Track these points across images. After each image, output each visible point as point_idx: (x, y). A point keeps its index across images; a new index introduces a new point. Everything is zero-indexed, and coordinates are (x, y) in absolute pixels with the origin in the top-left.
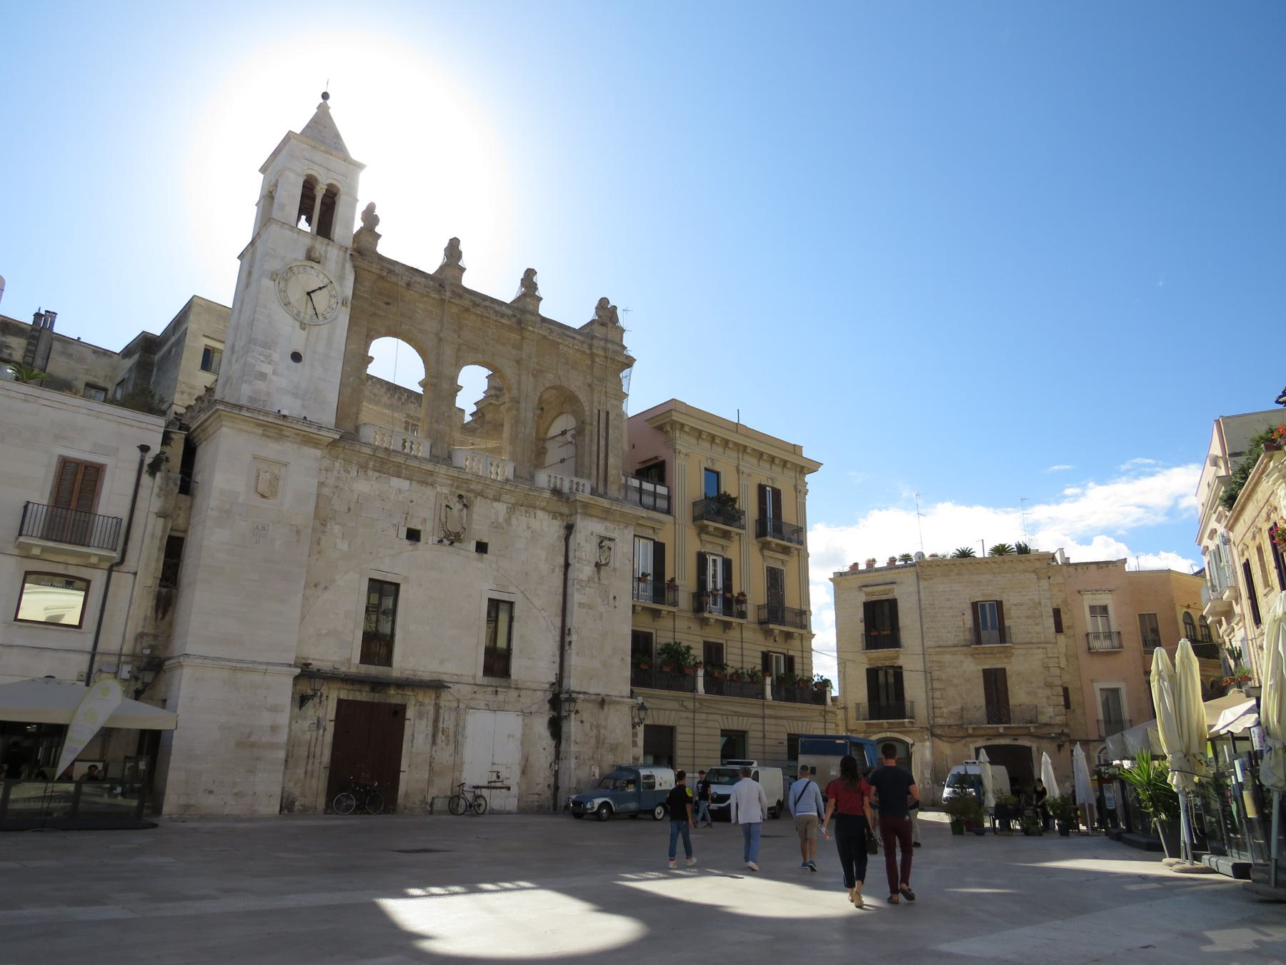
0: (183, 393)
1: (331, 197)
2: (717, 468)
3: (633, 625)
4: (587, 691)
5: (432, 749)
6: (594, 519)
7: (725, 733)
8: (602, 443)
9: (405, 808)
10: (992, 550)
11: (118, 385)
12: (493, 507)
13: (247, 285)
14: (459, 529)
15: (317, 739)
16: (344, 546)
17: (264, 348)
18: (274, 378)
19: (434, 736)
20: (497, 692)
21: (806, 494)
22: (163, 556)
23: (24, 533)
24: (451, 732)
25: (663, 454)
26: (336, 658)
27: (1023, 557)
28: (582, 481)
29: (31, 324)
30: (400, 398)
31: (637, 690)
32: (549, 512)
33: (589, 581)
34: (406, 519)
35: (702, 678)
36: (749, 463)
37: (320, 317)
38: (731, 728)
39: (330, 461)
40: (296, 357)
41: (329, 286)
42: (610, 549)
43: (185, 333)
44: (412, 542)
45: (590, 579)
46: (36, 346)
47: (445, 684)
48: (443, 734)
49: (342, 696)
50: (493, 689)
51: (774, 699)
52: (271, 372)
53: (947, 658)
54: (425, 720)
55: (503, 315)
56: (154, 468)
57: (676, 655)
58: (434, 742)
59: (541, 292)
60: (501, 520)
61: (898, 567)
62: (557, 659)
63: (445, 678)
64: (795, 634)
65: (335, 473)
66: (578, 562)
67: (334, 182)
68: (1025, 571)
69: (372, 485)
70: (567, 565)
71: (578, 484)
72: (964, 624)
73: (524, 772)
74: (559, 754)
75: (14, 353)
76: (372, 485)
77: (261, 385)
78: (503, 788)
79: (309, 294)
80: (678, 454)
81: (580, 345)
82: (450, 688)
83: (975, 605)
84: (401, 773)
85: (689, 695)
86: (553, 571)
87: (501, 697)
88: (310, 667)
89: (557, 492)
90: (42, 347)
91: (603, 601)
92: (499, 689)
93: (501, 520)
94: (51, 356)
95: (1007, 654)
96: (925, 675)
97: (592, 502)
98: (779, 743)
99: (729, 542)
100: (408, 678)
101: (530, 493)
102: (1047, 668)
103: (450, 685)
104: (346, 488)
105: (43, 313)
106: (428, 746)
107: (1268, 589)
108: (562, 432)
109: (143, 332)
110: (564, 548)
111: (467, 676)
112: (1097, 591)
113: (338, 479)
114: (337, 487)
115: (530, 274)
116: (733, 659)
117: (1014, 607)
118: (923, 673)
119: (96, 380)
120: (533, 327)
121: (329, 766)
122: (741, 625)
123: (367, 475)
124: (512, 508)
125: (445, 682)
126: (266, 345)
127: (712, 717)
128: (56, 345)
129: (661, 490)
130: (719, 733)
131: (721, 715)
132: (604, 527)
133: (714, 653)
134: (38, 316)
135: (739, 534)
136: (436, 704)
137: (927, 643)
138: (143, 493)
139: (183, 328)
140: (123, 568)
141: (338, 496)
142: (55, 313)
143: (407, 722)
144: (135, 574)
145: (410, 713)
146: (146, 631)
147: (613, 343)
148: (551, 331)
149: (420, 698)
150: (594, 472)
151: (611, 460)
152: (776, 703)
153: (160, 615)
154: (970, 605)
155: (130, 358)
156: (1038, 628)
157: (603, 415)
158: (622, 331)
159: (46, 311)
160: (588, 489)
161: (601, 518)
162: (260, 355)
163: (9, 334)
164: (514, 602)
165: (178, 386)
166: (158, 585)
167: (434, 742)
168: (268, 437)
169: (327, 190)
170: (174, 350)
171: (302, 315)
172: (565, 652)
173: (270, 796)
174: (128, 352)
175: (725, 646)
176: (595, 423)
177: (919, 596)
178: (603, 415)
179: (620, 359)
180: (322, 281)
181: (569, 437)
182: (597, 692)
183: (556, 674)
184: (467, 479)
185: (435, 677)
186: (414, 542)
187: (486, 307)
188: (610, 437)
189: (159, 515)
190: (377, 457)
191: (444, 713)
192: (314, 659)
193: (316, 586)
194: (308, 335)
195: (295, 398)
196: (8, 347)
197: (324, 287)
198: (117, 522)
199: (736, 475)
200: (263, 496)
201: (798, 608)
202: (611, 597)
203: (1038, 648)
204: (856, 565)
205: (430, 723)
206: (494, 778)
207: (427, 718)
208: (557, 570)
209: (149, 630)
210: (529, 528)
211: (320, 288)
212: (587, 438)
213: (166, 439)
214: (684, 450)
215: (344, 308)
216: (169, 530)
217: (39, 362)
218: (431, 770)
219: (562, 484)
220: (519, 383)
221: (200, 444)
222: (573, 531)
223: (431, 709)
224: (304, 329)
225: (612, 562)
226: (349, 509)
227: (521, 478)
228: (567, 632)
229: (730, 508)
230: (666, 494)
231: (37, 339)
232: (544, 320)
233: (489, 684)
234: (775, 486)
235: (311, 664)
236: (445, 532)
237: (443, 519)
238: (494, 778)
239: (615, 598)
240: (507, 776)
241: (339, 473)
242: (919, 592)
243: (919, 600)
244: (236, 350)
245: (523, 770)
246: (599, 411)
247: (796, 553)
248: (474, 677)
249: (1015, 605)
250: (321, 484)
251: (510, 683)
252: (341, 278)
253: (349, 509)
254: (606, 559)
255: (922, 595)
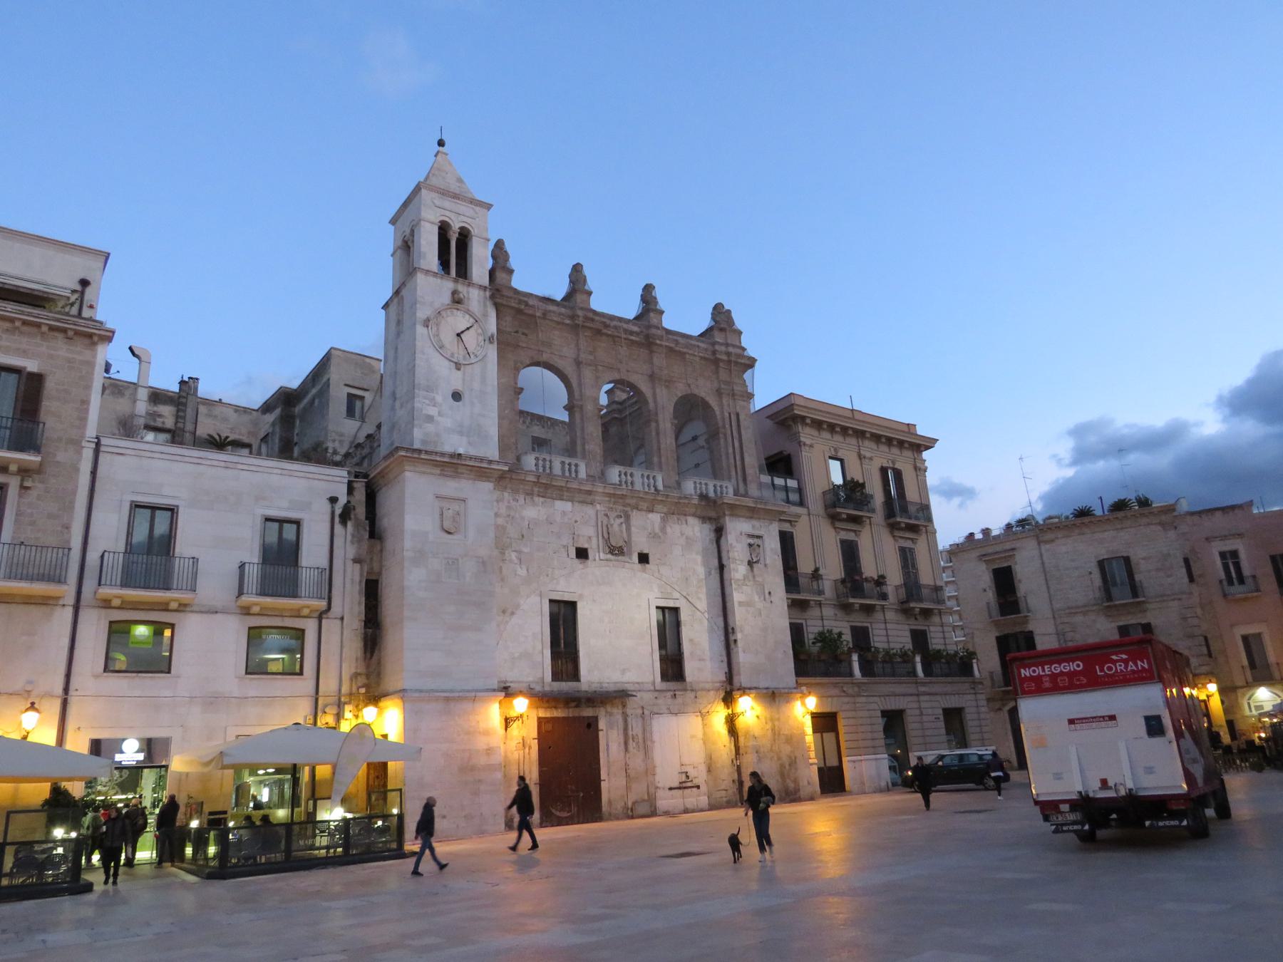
0: (334, 441)
1: (464, 237)
2: (840, 455)
3: (790, 618)
4: (757, 686)
5: (625, 756)
6: (742, 519)
7: (885, 713)
8: (737, 444)
9: (610, 814)
10: (1112, 506)
11: (262, 440)
12: (648, 518)
13: (398, 334)
14: (621, 543)
15: (524, 757)
16: (522, 572)
17: (428, 391)
18: (439, 419)
19: (626, 743)
20: (675, 695)
21: (925, 471)
22: (363, 599)
23: (103, 582)
24: (640, 736)
25: (788, 448)
26: (531, 679)
27: (1146, 510)
28: (725, 484)
29: (178, 391)
30: (524, 422)
31: (802, 680)
32: (699, 517)
33: (744, 580)
34: (573, 538)
35: (857, 663)
36: (868, 448)
37: (472, 356)
38: (950, 706)
39: (499, 493)
40: (457, 396)
41: (475, 326)
42: (759, 546)
43: (328, 384)
44: (582, 560)
45: (745, 577)
46: (184, 411)
47: (630, 693)
48: (633, 741)
49: (540, 715)
50: (672, 693)
51: (863, 676)
52: (437, 414)
53: (1079, 619)
54: (616, 728)
55: (632, 333)
56: (345, 516)
57: (828, 640)
58: (626, 749)
59: (662, 304)
60: (657, 530)
61: (1015, 533)
62: (725, 659)
63: (629, 687)
64: (812, 602)
65: (506, 504)
66: (733, 563)
67: (447, 219)
68: (1149, 524)
69: (539, 510)
70: (721, 567)
71: (721, 486)
72: (1092, 583)
73: (709, 771)
74: (739, 749)
75: (166, 420)
76: (539, 510)
77: (430, 428)
78: (693, 787)
79: (458, 335)
80: (803, 447)
81: (704, 352)
82: (636, 696)
83: (1101, 564)
84: (602, 783)
85: (848, 679)
86: (710, 573)
87: (679, 700)
88: (510, 689)
89: (703, 497)
90: (190, 412)
91: (760, 598)
92: (677, 693)
93: (657, 530)
94: (199, 419)
95: (1140, 607)
96: (1058, 638)
97: (737, 503)
98: (936, 718)
99: (858, 526)
100: (595, 692)
101: (681, 501)
102: (1185, 619)
103: (634, 693)
104: (517, 516)
105: (187, 380)
106: (622, 754)
107: (127, 393)
108: (693, 438)
109: (281, 388)
110: (716, 550)
111: (647, 683)
112: (1225, 536)
113: (509, 508)
114: (509, 516)
115: (648, 289)
116: (878, 640)
117: (1143, 562)
118: (1056, 636)
119: (241, 437)
120: (661, 340)
121: (538, 782)
122: (883, 606)
123: (533, 501)
124: (664, 520)
125: (629, 691)
126: (429, 389)
127: (872, 699)
128: (202, 409)
129: (792, 483)
130: (880, 714)
131: (879, 696)
132: (751, 526)
133: (861, 636)
134: (182, 383)
135: (870, 518)
136: (623, 713)
137: (1057, 606)
138: (338, 542)
139: (325, 379)
140: (331, 614)
141: (512, 524)
142: (197, 379)
143: (600, 733)
144: (342, 619)
145: (602, 724)
146: (359, 671)
147: (734, 346)
148: (677, 342)
149: (609, 709)
150: (733, 473)
151: (747, 460)
152: (929, 679)
153: (368, 655)
154: (1096, 564)
155: (271, 413)
156: (1169, 580)
157: (733, 417)
158: (740, 333)
159: (189, 378)
160: (731, 491)
161: (747, 518)
162: (425, 399)
163: (159, 403)
164: (679, 608)
165: (329, 435)
166: (363, 628)
167: (626, 749)
168: (446, 476)
169: (460, 234)
170: (317, 401)
171: (456, 355)
172: (731, 651)
173: (495, 815)
174: (267, 408)
175: (870, 630)
176: (727, 426)
177: (1042, 559)
178: (733, 417)
179: (743, 361)
180: (468, 321)
181: (701, 442)
182: (766, 686)
183: (726, 673)
184: (623, 495)
185: (620, 687)
186: (583, 560)
187: (616, 327)
188: (743, 438)
189: (356, 561)
190: (542, 483)
191: (632, 720)
192: (511, 682)
193: (504, 612)
194: (464, 374)
195: (461, 436)
196: (160, 416)
197: (471, 327)
198: (193, 562)
199: (859, 462)
200: (449, 533)
201: (933, 584)
202: (767, 592)
203: (1174, 600)
204: (972, 535)
205: (621, 731)
206: (684, 778)
207: (618, 727)
208: (713, 572)
209: (362, 670)
210: (682, 534)
211: (468, 329)
212: (722, 441)
213: (350, 490)
214: (808, 442)
215: (490, 346)
216: (365, 574)
217: (189, 427)
218: (628, 776)
219: (706, 489)
220: (654, 395)
221: (378, 490)
222: (723, 533)
223: (620, 718)
224: (459, 369)
225: (762, 559)
226: (523, 536)
227: (670, 487)
228: (730, 630)
229: (858, 494)
230: (797, 486)
231: (185, 405)
232: (668, 332)
233: (668, 689)
234: (896, 467)
235: (510, 687)
236: (609, 547)
237: (606, 535)
238: (684, 778)
239: (770, 593)
240: (696, 776)
241: (509, 502)
242: (1041, 555)
243: (1043, 563)
244: (398, 396)
245: (709, 768)
246: (730, 414)
247: (868, 521)
248: (654, 683)
249: (1143, 559)
250: (497, 515)
251: (686, 686)
252: (485, 315)
253: (523, 536)
254: (757, 557)
255: (1045, 558)
